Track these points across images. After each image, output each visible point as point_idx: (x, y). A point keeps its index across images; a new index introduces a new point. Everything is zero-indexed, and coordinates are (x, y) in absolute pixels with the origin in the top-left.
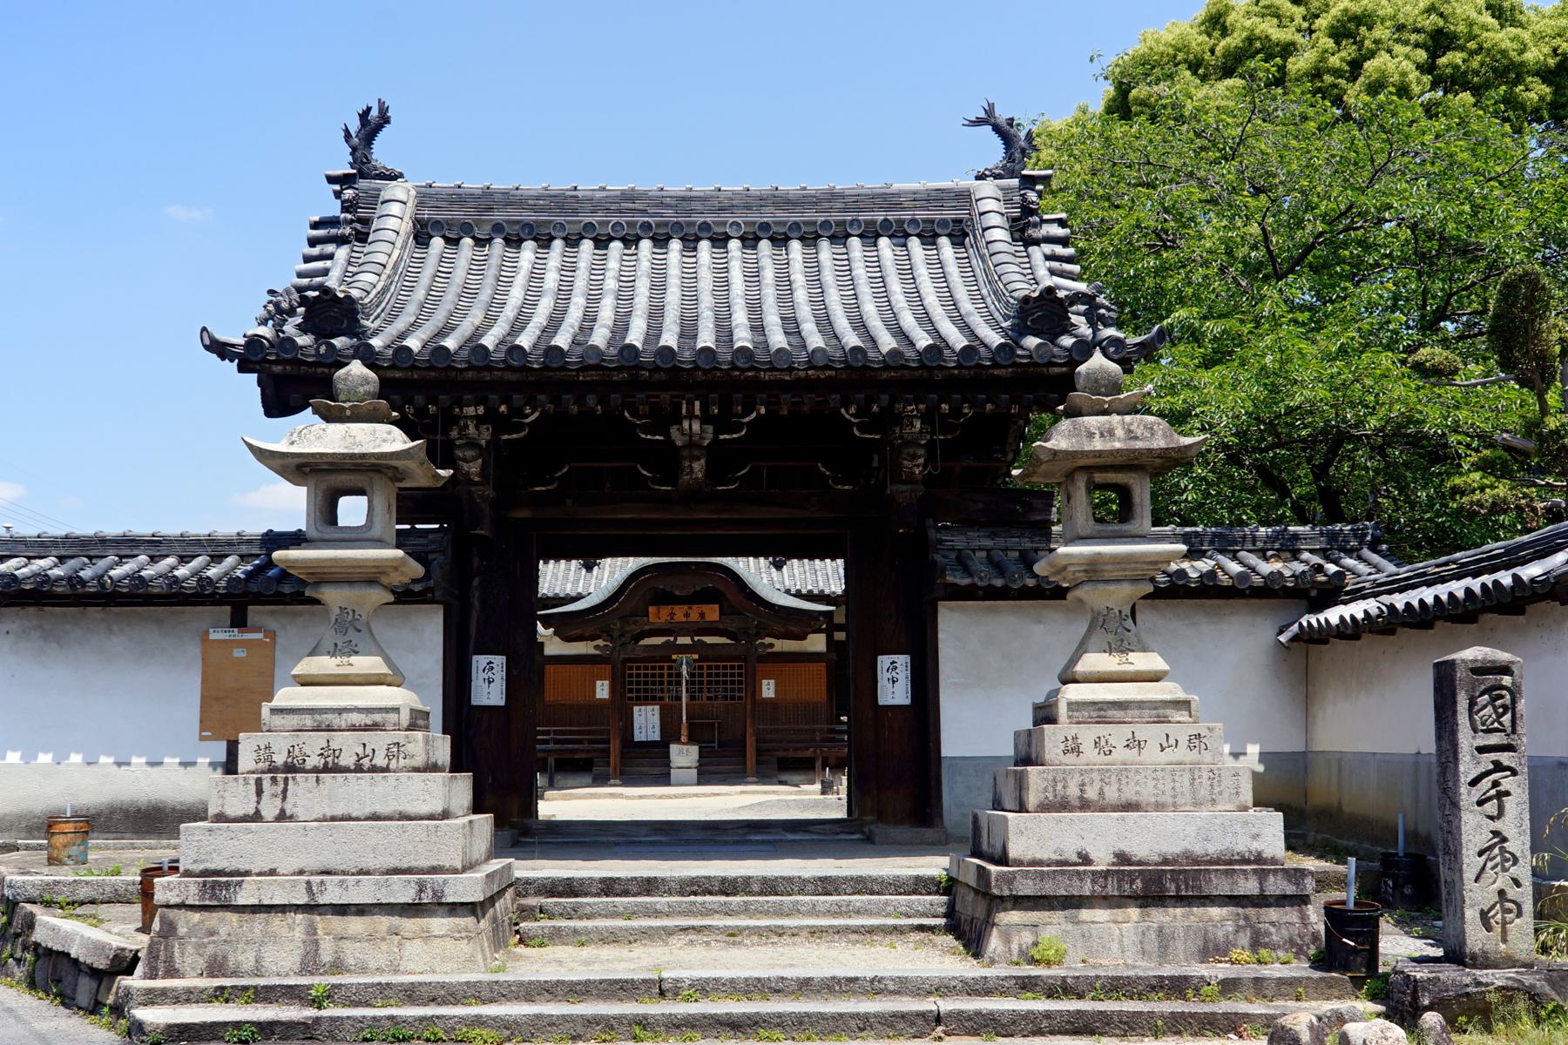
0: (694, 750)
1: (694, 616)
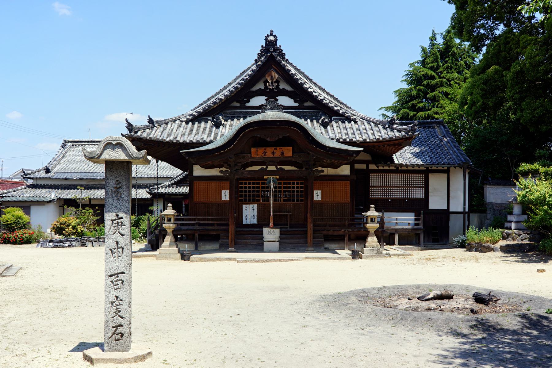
0: (277, 231)
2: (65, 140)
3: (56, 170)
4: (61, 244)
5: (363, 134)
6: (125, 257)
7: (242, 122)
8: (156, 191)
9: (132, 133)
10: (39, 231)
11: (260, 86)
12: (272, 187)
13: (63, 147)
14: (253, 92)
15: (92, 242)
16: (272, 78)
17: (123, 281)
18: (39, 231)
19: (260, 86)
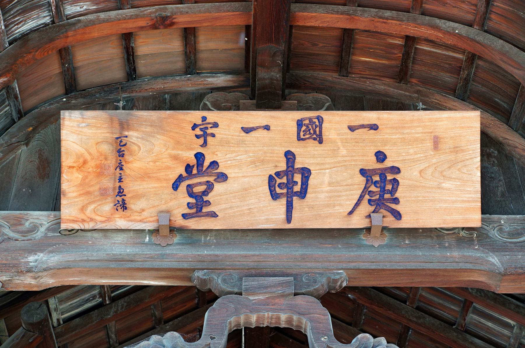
1: (333, 198)
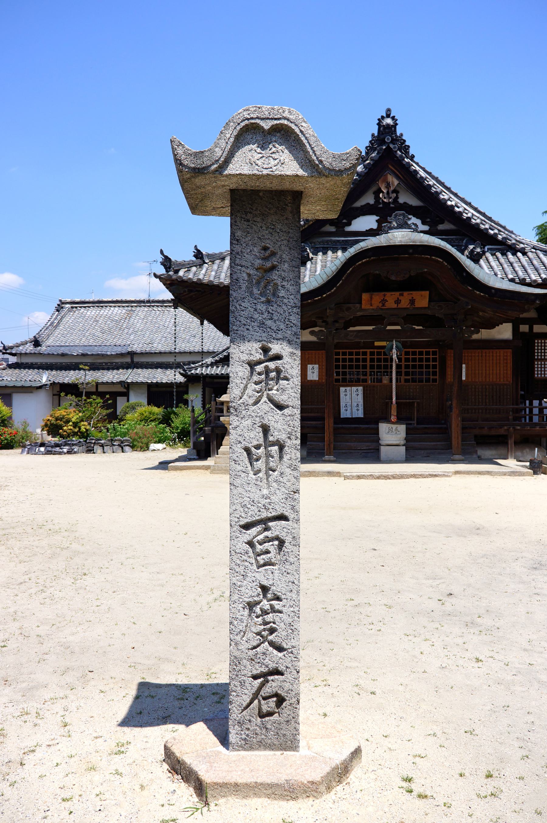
0: (402, 428)
1: (405, 303)
2: (60, 301)
3: (50, 342)
4: (58, 449)
5: (541, 271)
6: (288, 471)
7: (341, 256)
8: (193, 372)
9: (171, 273)
10: (24, 430)
11: (369, 199)
12: (395, 356)
13: (58, 311)
14: (357, 208)
15: (102, 446)
16: (388, 186)
17: (282, 543)
18: (24, 430)
19: (369, 199)
